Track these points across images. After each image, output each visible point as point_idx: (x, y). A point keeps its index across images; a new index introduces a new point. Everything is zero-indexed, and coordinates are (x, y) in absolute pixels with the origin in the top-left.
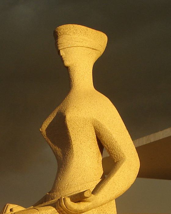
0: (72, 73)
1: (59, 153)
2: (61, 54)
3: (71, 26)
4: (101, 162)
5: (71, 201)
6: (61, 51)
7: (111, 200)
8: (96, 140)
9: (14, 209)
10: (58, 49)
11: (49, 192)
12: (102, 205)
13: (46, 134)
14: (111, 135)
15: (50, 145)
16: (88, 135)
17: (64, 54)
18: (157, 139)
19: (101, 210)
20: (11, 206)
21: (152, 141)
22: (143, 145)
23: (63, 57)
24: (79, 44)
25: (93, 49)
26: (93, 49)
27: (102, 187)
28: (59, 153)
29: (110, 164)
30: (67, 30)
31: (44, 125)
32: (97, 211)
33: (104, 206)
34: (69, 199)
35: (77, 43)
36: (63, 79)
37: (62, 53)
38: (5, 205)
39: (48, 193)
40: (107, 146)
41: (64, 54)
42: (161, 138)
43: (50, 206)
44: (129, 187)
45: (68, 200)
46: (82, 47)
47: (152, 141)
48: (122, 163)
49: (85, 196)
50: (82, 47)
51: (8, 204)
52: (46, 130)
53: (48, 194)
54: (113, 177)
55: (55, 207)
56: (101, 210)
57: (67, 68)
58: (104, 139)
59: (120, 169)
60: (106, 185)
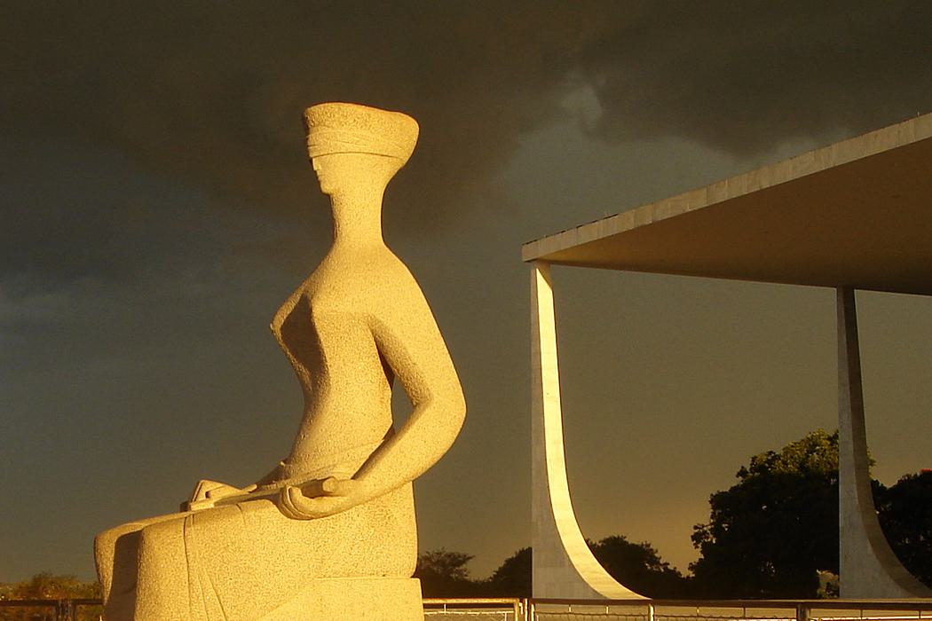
0: (336, 208)
1: (307, 379)
2: (315, 168)
3: (334, 106)
4: (390, 402)
5: (304, 495)
6: (314, 160)
7: (405, 482)
8: (377, 356)
9: (212, 493)
10: (308, 155)
11: (284, 459)
12: (373, 499)
13: (282, 338)
14: (404, 348)
15: (289, 359)
16: (360, 348)
17: (320, 168)
18: (779, 180)
19: (378, 506)
20: (208, 486)
21: (766, 185)
22: (739, 195)
23: (318, 174)
24: (350, 147)
25: (382, 155)
26: (382, 155)
27: (380, 459)
28: (307, 379)
29: (405, 403)
30: (326, 117)
31: (277, 317)
32: (366, 508)
33: (383, 498)
34: (300, 491)
35: (347, 145)
36: (318, 220)
37: (317, 165)
38: (198, 484)
39: (284, 462)
40: (398, 370)
41: (320, 168)
42: (789, 178)
43: (268, 501)
44: (436, 460)
45: (298, 493)
46: (360, 151)
47: (764, 187)
48: (424, 409)
49: (324, 489)
50: (360, 151)
51: (202, 481)
52: (281, 329)
53: (282, 463)
54: (400, 442)
55: (276, 503)
56: (378, 506)
57: (328, 196)
58: (391, 357)
59: (416, 423)
60: (385, 459)
